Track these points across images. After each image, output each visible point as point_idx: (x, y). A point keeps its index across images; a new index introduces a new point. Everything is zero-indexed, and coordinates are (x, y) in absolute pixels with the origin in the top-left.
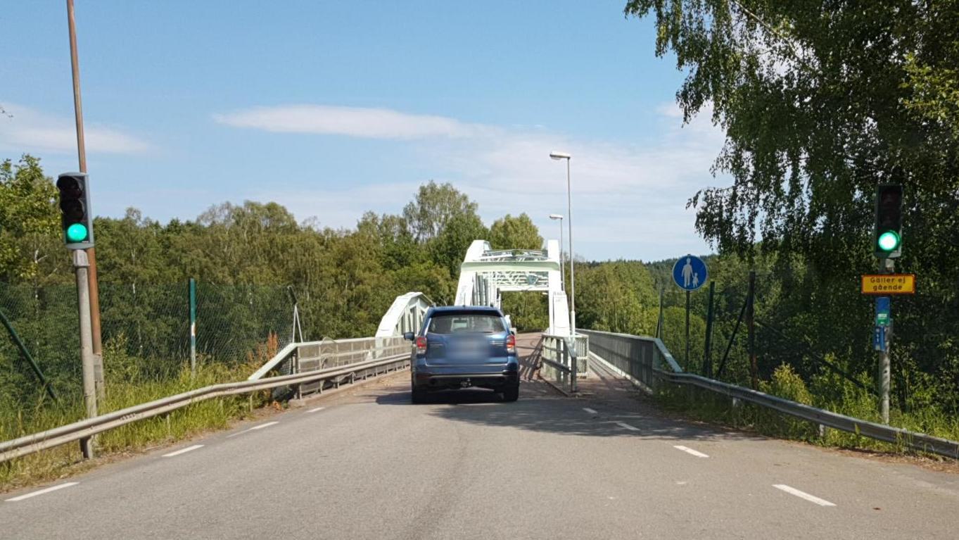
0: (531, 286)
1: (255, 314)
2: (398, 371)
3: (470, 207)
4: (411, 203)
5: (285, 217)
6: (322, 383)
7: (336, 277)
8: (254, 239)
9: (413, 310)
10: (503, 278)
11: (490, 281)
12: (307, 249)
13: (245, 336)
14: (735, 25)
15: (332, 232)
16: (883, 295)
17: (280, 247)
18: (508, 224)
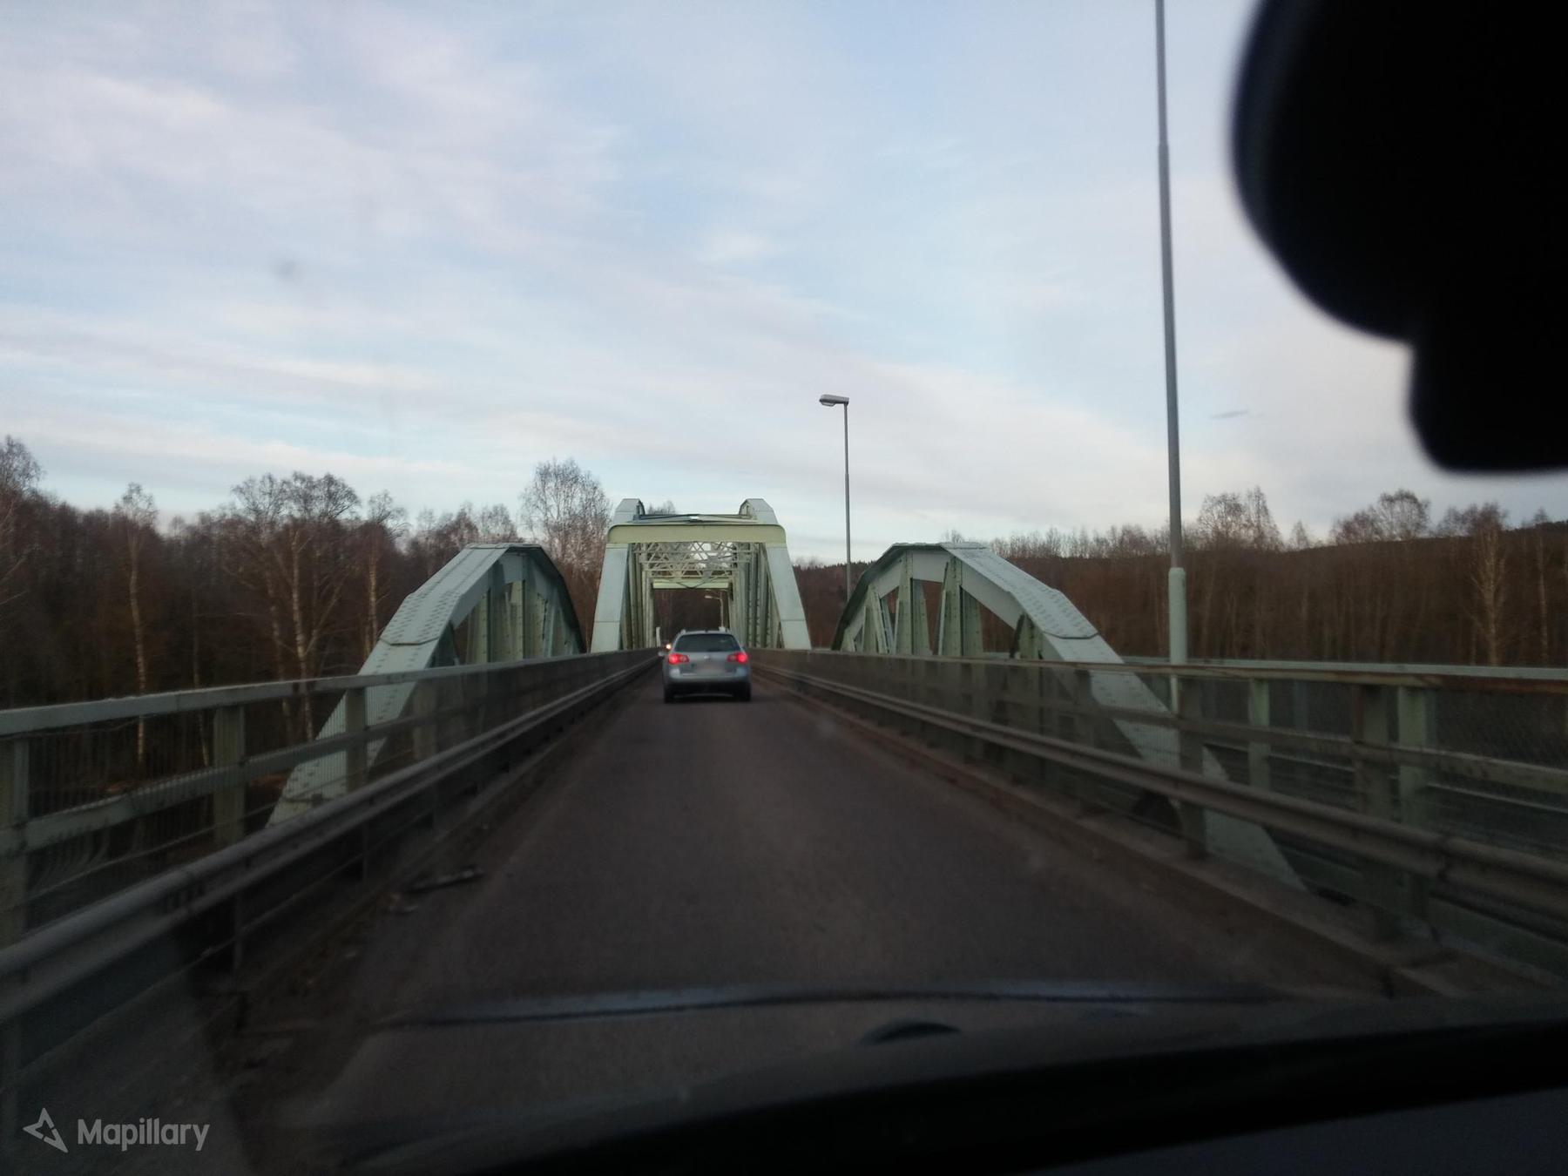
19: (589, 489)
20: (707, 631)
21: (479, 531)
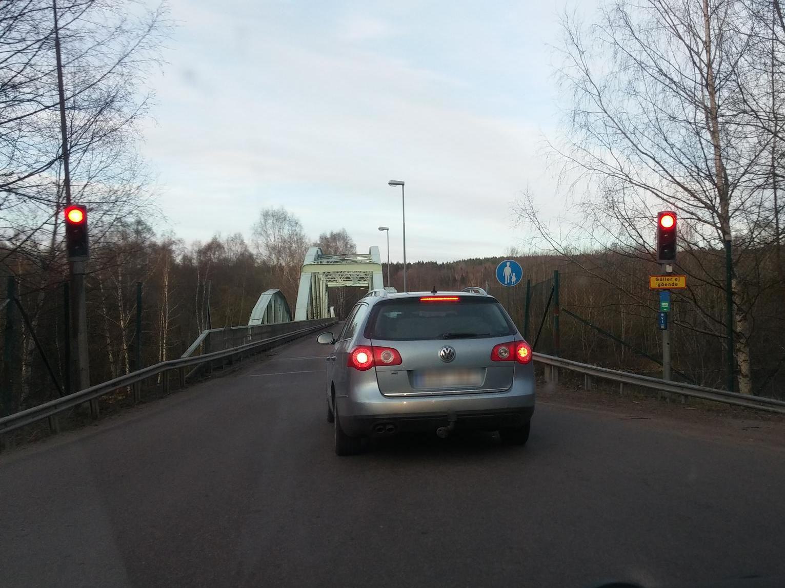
14: (23, 75)
16: (664, 289)
19: (293, 224)
20: (434, 291)
21: (226, 249)
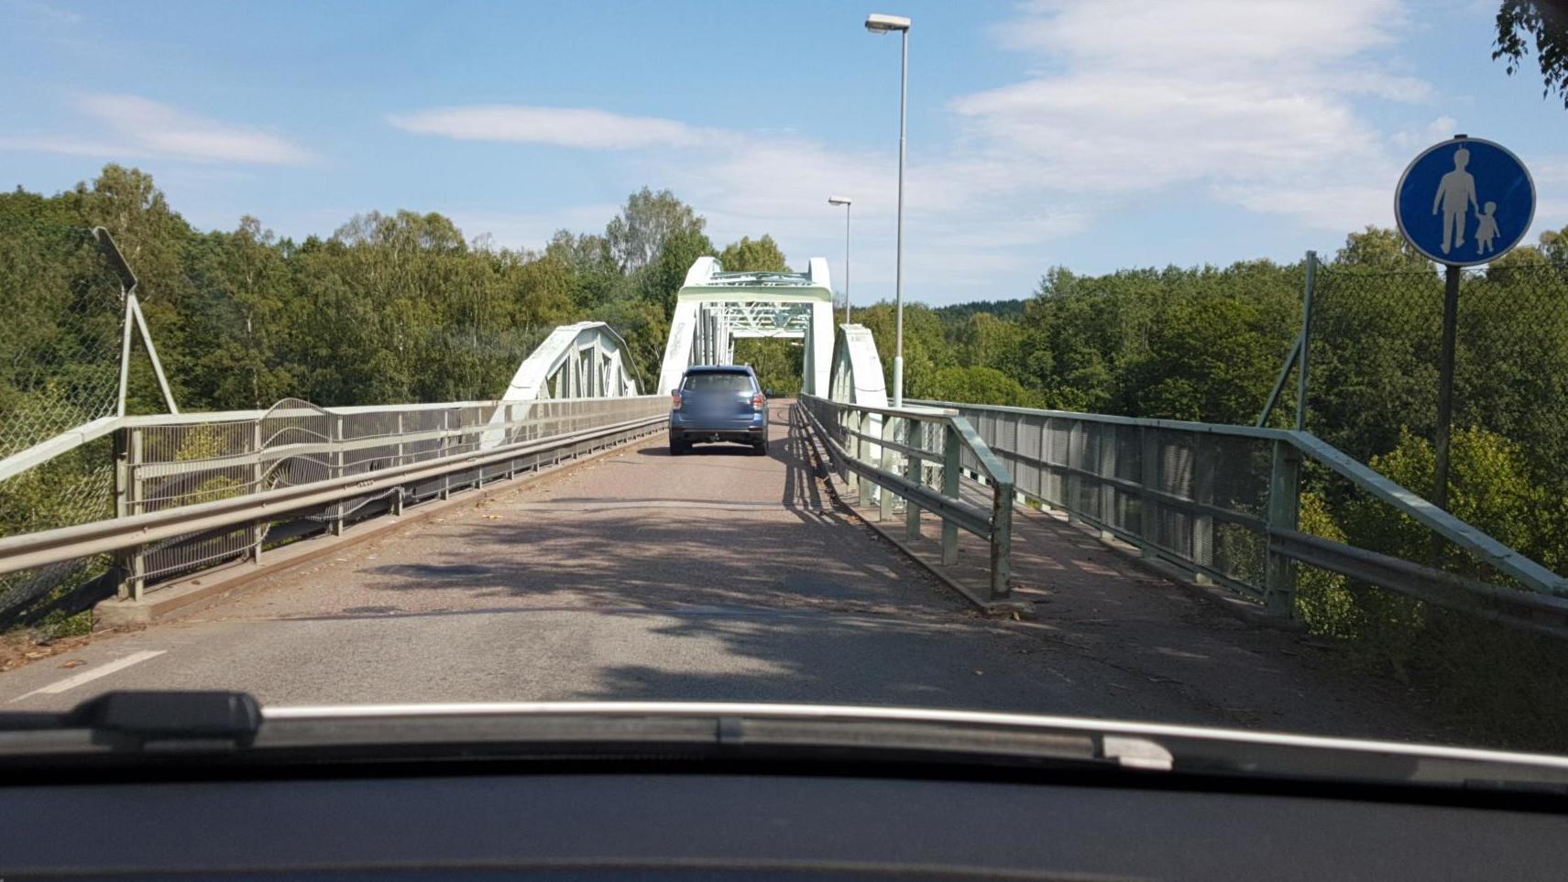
0: (779, 330)
1: (405, 363)
2: (540, 471)
3: (695, 224)
4: (617, 217)
5: (451, 233)
6: (260, 534)
7: (513, 316)
8: (406, 260)
9: (587, 354)
10: (740, 316)
11: (720, 320)
12: (476, 276)
13: (391, 393)
15: (511, 255)
17: (442, 274)
18: (746, 250)
